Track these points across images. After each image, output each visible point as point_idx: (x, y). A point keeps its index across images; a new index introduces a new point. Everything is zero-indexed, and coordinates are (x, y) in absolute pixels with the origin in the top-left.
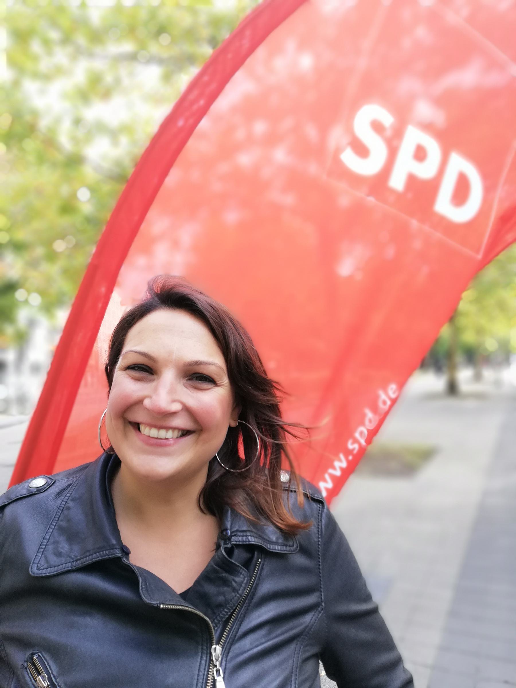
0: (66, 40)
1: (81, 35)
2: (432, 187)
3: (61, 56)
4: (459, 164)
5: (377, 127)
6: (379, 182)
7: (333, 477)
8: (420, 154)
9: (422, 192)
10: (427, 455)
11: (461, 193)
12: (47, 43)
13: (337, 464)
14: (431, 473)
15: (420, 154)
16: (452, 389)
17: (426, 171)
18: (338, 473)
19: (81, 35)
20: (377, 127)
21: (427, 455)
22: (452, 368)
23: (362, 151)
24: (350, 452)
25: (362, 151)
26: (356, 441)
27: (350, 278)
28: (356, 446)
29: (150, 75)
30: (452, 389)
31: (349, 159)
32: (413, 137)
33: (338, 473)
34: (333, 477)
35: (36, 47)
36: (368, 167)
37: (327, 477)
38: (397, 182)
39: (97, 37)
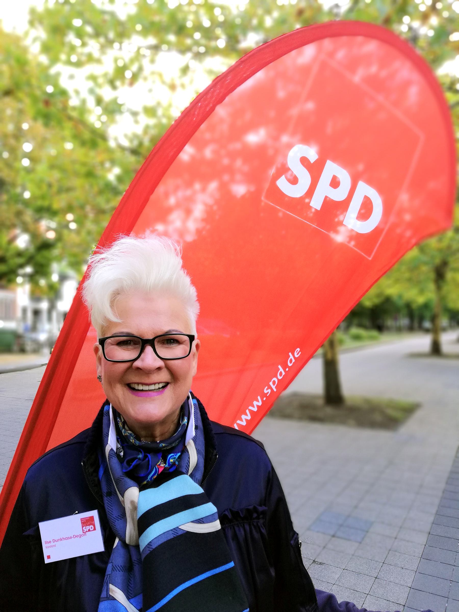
0: (97, 34)
1: (110, 30)
2: (344, 205)
3: (93, 46)
4: (364, 190)
5: (304, 161)
6: (301, 204)
7: (252, 412)
8: (335, 183)
9: (333, 209)
10: (409, 410)
11: (366, 211)
12: (80, 34)
13: (255, 403)
14: (410, 427)
15: (335, 183)
16: (436, 349)
17: (339, 195)
18: (255, 409)
19: (110, 30)
20: (304, 161)
21: (409, 410)
22: (435, 331)
23: (294, 181)
24: (264, 395)
25: (294, 181)
26: (270, 387)
27: (342, 246)
28: (269, 391)
29: (170, 61)
30: (436, 349)
31: (282, 184)
32: (332, 168)
33: (255, 409)
34: (252, 412)
35: (71, 38)
36: (295, 192)
37: (247, 411)
38: (316, 203)
39: (123, 31)
